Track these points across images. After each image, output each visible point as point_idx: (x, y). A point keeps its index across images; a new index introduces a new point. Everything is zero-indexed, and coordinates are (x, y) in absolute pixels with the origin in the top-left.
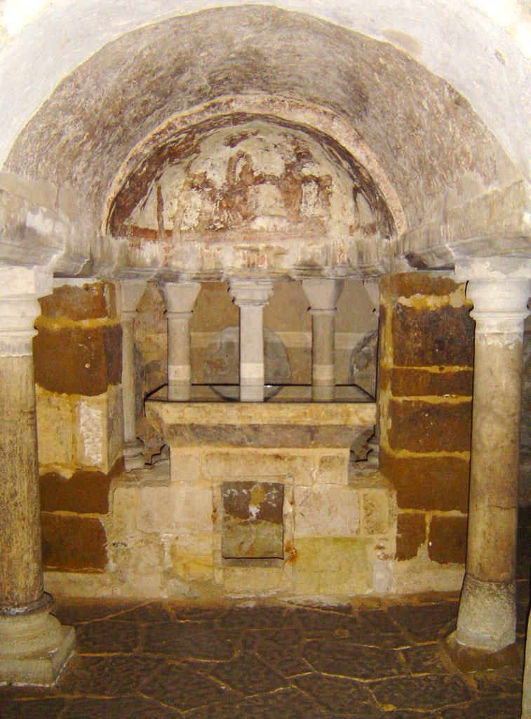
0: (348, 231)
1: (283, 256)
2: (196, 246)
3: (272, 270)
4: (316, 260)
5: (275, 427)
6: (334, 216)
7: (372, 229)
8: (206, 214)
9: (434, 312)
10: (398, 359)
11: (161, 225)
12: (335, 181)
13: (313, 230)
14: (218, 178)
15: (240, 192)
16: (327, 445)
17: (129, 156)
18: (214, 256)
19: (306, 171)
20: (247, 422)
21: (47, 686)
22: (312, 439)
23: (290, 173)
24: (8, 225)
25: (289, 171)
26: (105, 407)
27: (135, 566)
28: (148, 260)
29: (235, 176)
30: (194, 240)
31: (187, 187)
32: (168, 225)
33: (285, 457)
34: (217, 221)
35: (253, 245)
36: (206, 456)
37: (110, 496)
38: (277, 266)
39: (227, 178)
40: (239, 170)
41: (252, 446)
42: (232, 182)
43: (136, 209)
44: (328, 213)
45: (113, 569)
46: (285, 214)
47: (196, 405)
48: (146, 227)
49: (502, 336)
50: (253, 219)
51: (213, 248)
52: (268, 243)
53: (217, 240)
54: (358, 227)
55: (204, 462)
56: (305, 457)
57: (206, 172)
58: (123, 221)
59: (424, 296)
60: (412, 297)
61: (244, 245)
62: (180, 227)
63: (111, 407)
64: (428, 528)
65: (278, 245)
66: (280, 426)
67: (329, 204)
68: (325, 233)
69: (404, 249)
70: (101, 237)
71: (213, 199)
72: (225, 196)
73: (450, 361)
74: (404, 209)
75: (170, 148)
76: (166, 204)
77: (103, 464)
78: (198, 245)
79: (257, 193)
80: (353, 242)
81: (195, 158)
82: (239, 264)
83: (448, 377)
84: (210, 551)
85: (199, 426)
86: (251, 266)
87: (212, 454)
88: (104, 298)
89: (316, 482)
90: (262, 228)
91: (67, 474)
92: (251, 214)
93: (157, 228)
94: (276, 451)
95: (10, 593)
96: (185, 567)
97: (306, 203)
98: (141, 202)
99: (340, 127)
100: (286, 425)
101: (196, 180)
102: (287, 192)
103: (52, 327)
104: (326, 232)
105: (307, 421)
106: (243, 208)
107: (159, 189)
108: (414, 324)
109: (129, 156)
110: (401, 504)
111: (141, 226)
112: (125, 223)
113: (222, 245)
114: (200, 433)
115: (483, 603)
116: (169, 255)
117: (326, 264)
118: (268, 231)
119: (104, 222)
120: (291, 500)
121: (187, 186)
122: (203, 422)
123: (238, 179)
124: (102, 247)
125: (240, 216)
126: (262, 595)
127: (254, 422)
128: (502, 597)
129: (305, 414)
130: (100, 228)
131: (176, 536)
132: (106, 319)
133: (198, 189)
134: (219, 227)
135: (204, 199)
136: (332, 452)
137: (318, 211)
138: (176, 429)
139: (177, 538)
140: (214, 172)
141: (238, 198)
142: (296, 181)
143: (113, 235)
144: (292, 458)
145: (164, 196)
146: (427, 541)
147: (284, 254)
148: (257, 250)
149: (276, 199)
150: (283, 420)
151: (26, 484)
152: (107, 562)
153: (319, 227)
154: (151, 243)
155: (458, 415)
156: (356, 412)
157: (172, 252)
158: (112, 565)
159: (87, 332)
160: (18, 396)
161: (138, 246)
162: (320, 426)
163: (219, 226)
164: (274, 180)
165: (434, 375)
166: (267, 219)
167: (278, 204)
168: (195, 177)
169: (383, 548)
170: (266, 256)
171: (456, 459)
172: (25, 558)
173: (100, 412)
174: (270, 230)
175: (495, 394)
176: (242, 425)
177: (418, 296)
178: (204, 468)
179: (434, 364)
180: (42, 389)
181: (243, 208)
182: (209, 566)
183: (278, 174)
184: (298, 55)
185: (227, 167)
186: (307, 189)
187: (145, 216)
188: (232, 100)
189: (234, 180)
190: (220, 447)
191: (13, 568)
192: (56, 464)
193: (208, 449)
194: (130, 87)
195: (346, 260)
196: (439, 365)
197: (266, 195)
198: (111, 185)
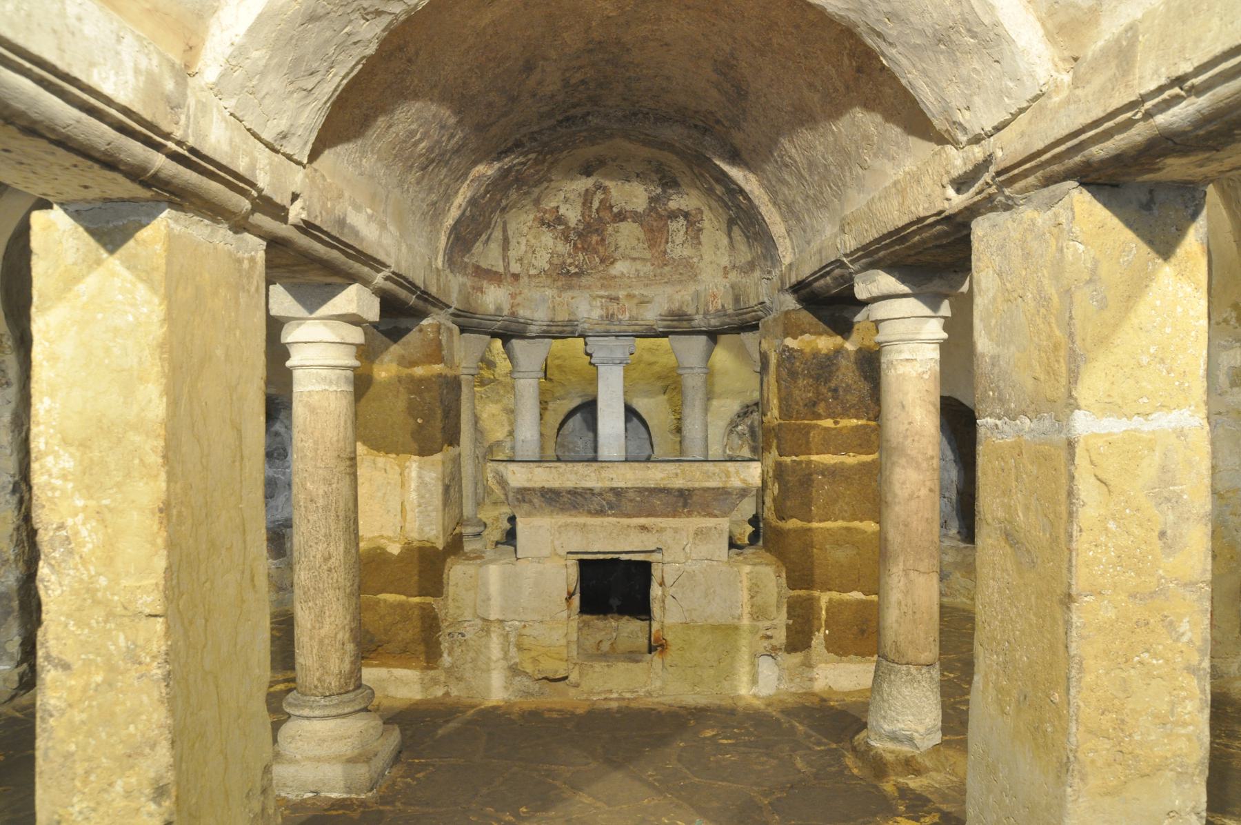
0: (721, 273)
4: (685, 308)
5: (641, 491)
6: (705, 257)
7: (751, 266)
8: (559, 256)
9: (826, 355)
10: (786, 412)
11: (507, 267)
12: (707, 214)
13: (681, 274)
14: (573, 215)
15: (597, 230)
17: (471, 177)
19: (673, 205)
20: (608, 484)
21: (363, 796)
22: (685, 505)
23: (655, 207)
24: (324, 213)
26: (440, 469)
27: (473, 660)
29: (591, 211)
31: (536, 224)
32: (515, 268)
34: (570, 265)
35: (613, 293)
36: (560, 527)
37: (445, 576)
38: (640, 317)
39: (583, 215)
40: (596, 205)
41: (614, 515)
42: (588, 219)
43: (478, 244)
44: (698, 254)
45: (447, 665)
46: (648, 256)
47: (547, 464)
48: (489, 267)
49: (915, 362)
50: (612, 263)
51: (567, 295)
52: (629, 290)
53: (570, 287)
54: (734, 267)
55: (557, 536)
57: (558, 207)
58: (464, 256)
59: (813, 337)
60: (800, 338)
61: (602, 293)
62: (528, 270)
63: (448, 470)
64: (824, 612)
65: (642, 292)
66: (647, 489)
67: (700, 243)
68: (694, 277)
69: (790, 279)
70: (437, 269)
71: (567, 239)
72: (580, 235)
73: (845, 414)
74: (789, 235)
75: (518, 170)
76: (513, 242)
77: (437, 538)
78: (549, 292)
79: (617, 232)
81: (546, 189)
82: (596, 314)
83: (844, 431)
84: (563, 642)
85: (551, 490)
86: (610, 317)
87: (567, 525)
88: (440, 340)
89: (689, 558)
90: (622, 273)
91: (395, 549)
92: (609, 257)
93: (501, 270)
94: (642, 521)
95: (319, 680)
96: (535, 660)
97: (673, 242)
98: (484, 237)
99: (713, 142)
100: (655, 488)
101: (547, 216)
102: (652, 231)
103: (379, 375)
105: (679, 483)
106: (601, 249)
107: (505, 223)
108: (803, 371)
110: (792, 585)
111: (484, 265)
112: (466, 260)
113: (576, 293)
114: (553, 498)
115: (899, 692)
116: (516, 301)
117: (697, 313)
119: (441, 253)
120: (660, 580)
121: (536, 223)
122: (556, 484)
123: (594, 215)
124: (438, 280)
125: (597, 259)
126: (628, 695)
127: (615, 485)
128: (923, 683)
129: (677, 475)
130: (436, 259)
132: (441, 366)
133: (549, 226)
135: (556, 238)
137: (687, 252)
139: (525, 626)
140: (568, 206)
141: (595, 238)
142: (660, 217)
143: (452, 272)
144: (661, 530)
145: (510, 233)
146: (822, 630)
147: (648, 302)
148: (616, 299)
149: (639, 239)
151: (342, 545)
152: (441, 656)
153: (688, 270)
155: (857, 477)
156: (737, 472)
157: (519, 299)
158: (446, 660)
159: (422, 380)
160: (335, 439)
161: (481, 290)
162: (694, 489)
163: (573, 270)
164: (636, 217)
165: (827, 429)
166: (628, 263)
167: (641, 245)
168: (545, 212)
169: (770, 637)
171: (856, 529)
172: (340, 636)
173: (434, 475)
175: (908, 433)
176: (601, 488)
177: (807, 337)
178: (556, 543)
179: (829, 416)
180: (365, 448)
181: (601, 249)
182: (561, 660)
183: (640, 210)
184: (666, 44)
185: (582, 200)
186: (673, 225)
187: (488, 254)
188: (588, 114)
189: (590, 216)
190: (576, 516)
191: (324, 648)
192: (382, 537)
193: (562, 519)
194: (471, 77)
195: (720, 307)
196: (833, 418)
197: (627, 235)
198: (449, 210)
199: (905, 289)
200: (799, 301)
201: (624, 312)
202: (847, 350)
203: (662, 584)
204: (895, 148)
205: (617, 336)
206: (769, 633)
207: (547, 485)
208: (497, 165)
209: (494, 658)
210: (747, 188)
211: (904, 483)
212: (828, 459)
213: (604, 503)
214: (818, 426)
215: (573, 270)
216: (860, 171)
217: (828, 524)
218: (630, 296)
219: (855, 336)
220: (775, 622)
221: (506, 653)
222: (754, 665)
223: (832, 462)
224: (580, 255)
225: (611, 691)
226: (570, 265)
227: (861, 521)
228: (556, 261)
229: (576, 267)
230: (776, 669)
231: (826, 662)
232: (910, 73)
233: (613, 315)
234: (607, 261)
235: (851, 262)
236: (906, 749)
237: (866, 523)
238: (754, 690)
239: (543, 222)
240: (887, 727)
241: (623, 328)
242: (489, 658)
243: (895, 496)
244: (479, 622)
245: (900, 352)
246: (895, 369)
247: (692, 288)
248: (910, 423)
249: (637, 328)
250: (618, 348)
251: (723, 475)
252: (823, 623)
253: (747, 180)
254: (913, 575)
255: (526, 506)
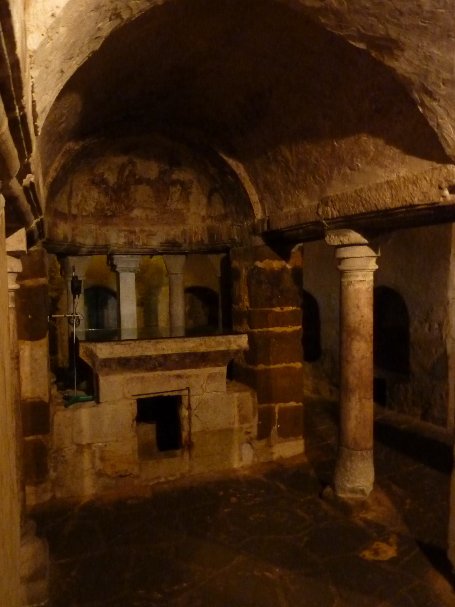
1: (153, 236)
2: (93, 227)
3: (145, 247)
4: (177, 240)
11: (70, 211)
14: (111, 178)
16: (213, 365)
17: (63, 150)
18: (105, 235)
19: (174, 177)
20: (162, 353)
25: (161, 176)
28: (61, 236)
30: (91, 223)
32: (74, 211)
33: (184, 376)
34: (108, 210)
39: (118, 179)
40: (127, 173)
41: (162, 370)
45: (53, 478)
49: (364, 282)
56: (197, 375)
59: (271, 261)
61: (124, 228)
62: (82, 213)
64: (277, 415)
71: (106, 194)
73: (287, 305)
76: (74, 194)
78: (93, 227)
80: (205, 227)
82: (122, 241)
86: (130, 244)
87: (132, 379)
93: (66, 211)
94: (178, 372)
96: (113, 466)
97: (172, 199)
104: (184, 220)
109: (63, 150)
110: (260, 401)
118: (141, 219)
126: (171, 478)
131: (104, 444)
134: (109, 214)
136: (217, 370)
138: (107, 363)
141: (123, 194)
144: (189, 377)
147: (153, 235)
150: (186, 349)
154: (63, 223)
156: (235, 341)
157: (77, 231)
158: (52, 474)
163: (109, 213)
164: (149, 182)
165: (277, 313)
168: (325, 202)
169: (249, 433)
170: (140, 237)
174: (143, 218)
175: (361, 322)
186: (173, 189)
190: (138, 372)
193: (129, 375)
195: (200, 239)
199: (365, 241)
200: (265, 241)
201: (139, 241)
202: (287, 268)
203: (189, 408)
204: (390, 161)
205: (131, 255)
206: (249, 430)
207: (123, 356)
208: (81, 143)
209: (86, 469)
210: (238, 172)
211: (358, 350)
212: (278, 329)
213: (157, 363)
214: (271, 311)
215: (109, 213)
216: (348, 171)
217: (278, 366)
218: (143, 231)
219: (292, 261)
220: (252, 424)
221: (93, 463)
222: (240, 449)
223: (280, 331)
224: (114, 204)
225: (159, 477)
226: (108, 210)
227: (294, 363)
228: (99, 207)
229: (111, 211)
230: (252, 450)
231: (279, 443)
232: (442, 119)
233: (132, 242)
234: (129, 208)
235: (328, 224)
236: (359, 496)
237: (296, 363)
238: (242, 464)
239: (93, 182)
240: (349, 486)
241: (139, 250)
242: (83, 469)
243: (353, 357)
244: (75, 447)
245: (357, 276)
246: (354, 286)
247: (181, 228)
248: (362, 316)
249: (146, 250)
250: (134, 262)
251: (228, 343)
252: (276, 421)
253: (238, 167)
254: (364, 401)
255: (106, 370)
